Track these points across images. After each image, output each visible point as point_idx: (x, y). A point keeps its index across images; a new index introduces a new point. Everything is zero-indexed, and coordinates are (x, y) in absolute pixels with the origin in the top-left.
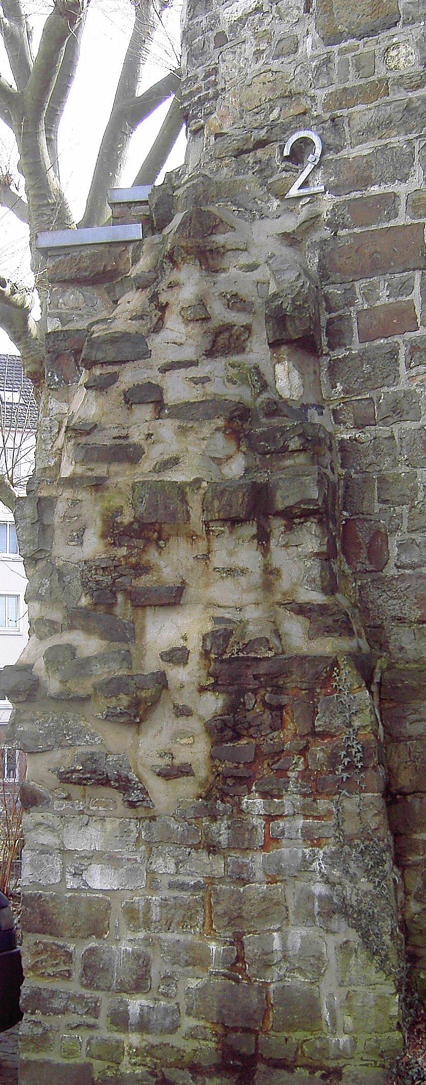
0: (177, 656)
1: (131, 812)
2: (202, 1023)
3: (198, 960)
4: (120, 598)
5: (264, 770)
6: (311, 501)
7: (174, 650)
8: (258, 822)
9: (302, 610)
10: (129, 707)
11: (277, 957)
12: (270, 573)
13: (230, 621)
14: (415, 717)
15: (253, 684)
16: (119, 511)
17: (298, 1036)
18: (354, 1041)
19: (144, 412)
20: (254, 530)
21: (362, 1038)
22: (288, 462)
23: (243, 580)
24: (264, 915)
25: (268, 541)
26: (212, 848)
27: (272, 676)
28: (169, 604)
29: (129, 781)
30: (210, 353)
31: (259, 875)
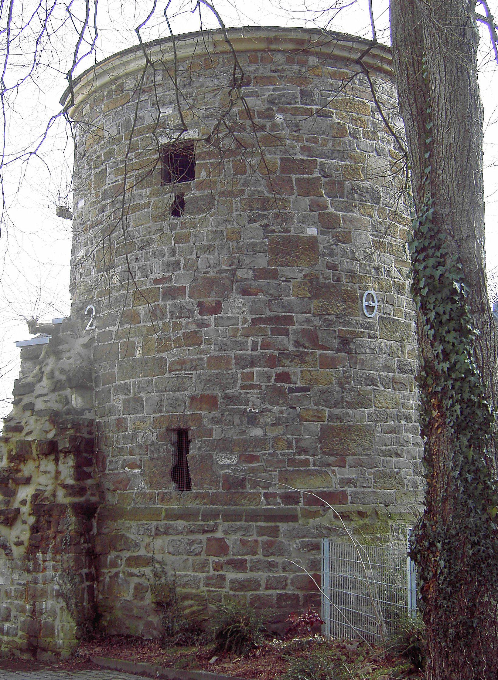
0: (23, 502)
1: (7, 557)
2: (23, 633)
3: (23, 611)
4: (10, 481)
5: (43, 544)
6: (66, 448)
7: (23, 500)
8: (41, 562)
9: (65, 487)
10: (4, 520)
11: (44, 611)
12: (58, 473)
13: (41, 490)
14: (105, 526)
15: (43, 514)
16: (12, 450)
17: (49, 639)
18: (64, 642)
19: (28, 413)
20: (54, 457)
21: (66, 641)
22: (68, 433)
23: (49, 475)
24: (42, 596)
25: (58, 461)
26: (29, 571)
27: (49, 511)
28: (24, 484)
29: (6, 546)
30: (53, 391)
31: (41, 582)
